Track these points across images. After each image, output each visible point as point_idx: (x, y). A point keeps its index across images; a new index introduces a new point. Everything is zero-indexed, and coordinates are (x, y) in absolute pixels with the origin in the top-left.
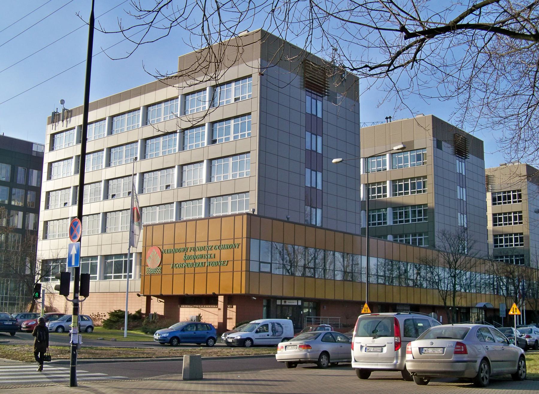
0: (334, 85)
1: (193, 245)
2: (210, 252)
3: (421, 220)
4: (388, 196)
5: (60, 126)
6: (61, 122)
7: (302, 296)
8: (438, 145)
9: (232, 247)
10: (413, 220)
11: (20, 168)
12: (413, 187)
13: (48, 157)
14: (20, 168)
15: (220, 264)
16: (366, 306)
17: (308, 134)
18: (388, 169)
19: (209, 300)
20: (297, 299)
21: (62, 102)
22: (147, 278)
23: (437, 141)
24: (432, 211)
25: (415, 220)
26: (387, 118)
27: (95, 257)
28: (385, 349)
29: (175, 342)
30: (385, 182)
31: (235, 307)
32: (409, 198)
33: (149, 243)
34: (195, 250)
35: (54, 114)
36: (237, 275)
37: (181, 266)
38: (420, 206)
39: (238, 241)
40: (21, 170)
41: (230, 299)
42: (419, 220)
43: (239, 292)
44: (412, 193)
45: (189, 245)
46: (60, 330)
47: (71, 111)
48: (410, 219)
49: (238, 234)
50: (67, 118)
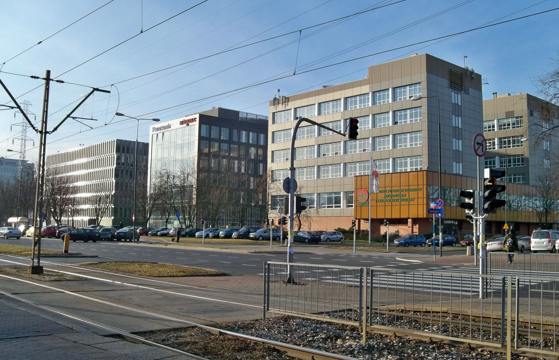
0: (466, 83)
1: (390, 189)
2: (402, 193)
3: (519, 165)
4: (496, 149)
5: (280, 107)
6: (280, 105)
7: (455, 218)
8: (531, 114)
9: (417, 190)
10: (514, 165)
11: (234, 130)
12: (514, 143)
13: (271, 128)
14: (234, 130)
15: (409, 200)
16: (506, 225)
17: (454, 116)
18: (496, 130)
19: (402, 221)
20: (451, 220)
21: (279, 91)
22: (359, 208)
23: (531, 111)
24: (527, 159)
25: (515, 165)
26: (494, 94)
27: (312, 194)
28: (545, 243)
29: (407, 245)
30: (494, 139)
31: (417, 225)
32: (512, 150)
33: (359, 187)
34: (391, 191)
35: (275, 99)
36: (420, 207)
37: (382, 201)
38: (518, 155)
39: (420, 187)
40: (235, 131)
41: (415, 221)
42: (518, 165)
43: (422, 217)
44: (513, 146)
45: (387, 189)
46: (328, 240)
47: (288, 98)
48: (512, 164)
49: (420, 183)
50: (285, 102)
